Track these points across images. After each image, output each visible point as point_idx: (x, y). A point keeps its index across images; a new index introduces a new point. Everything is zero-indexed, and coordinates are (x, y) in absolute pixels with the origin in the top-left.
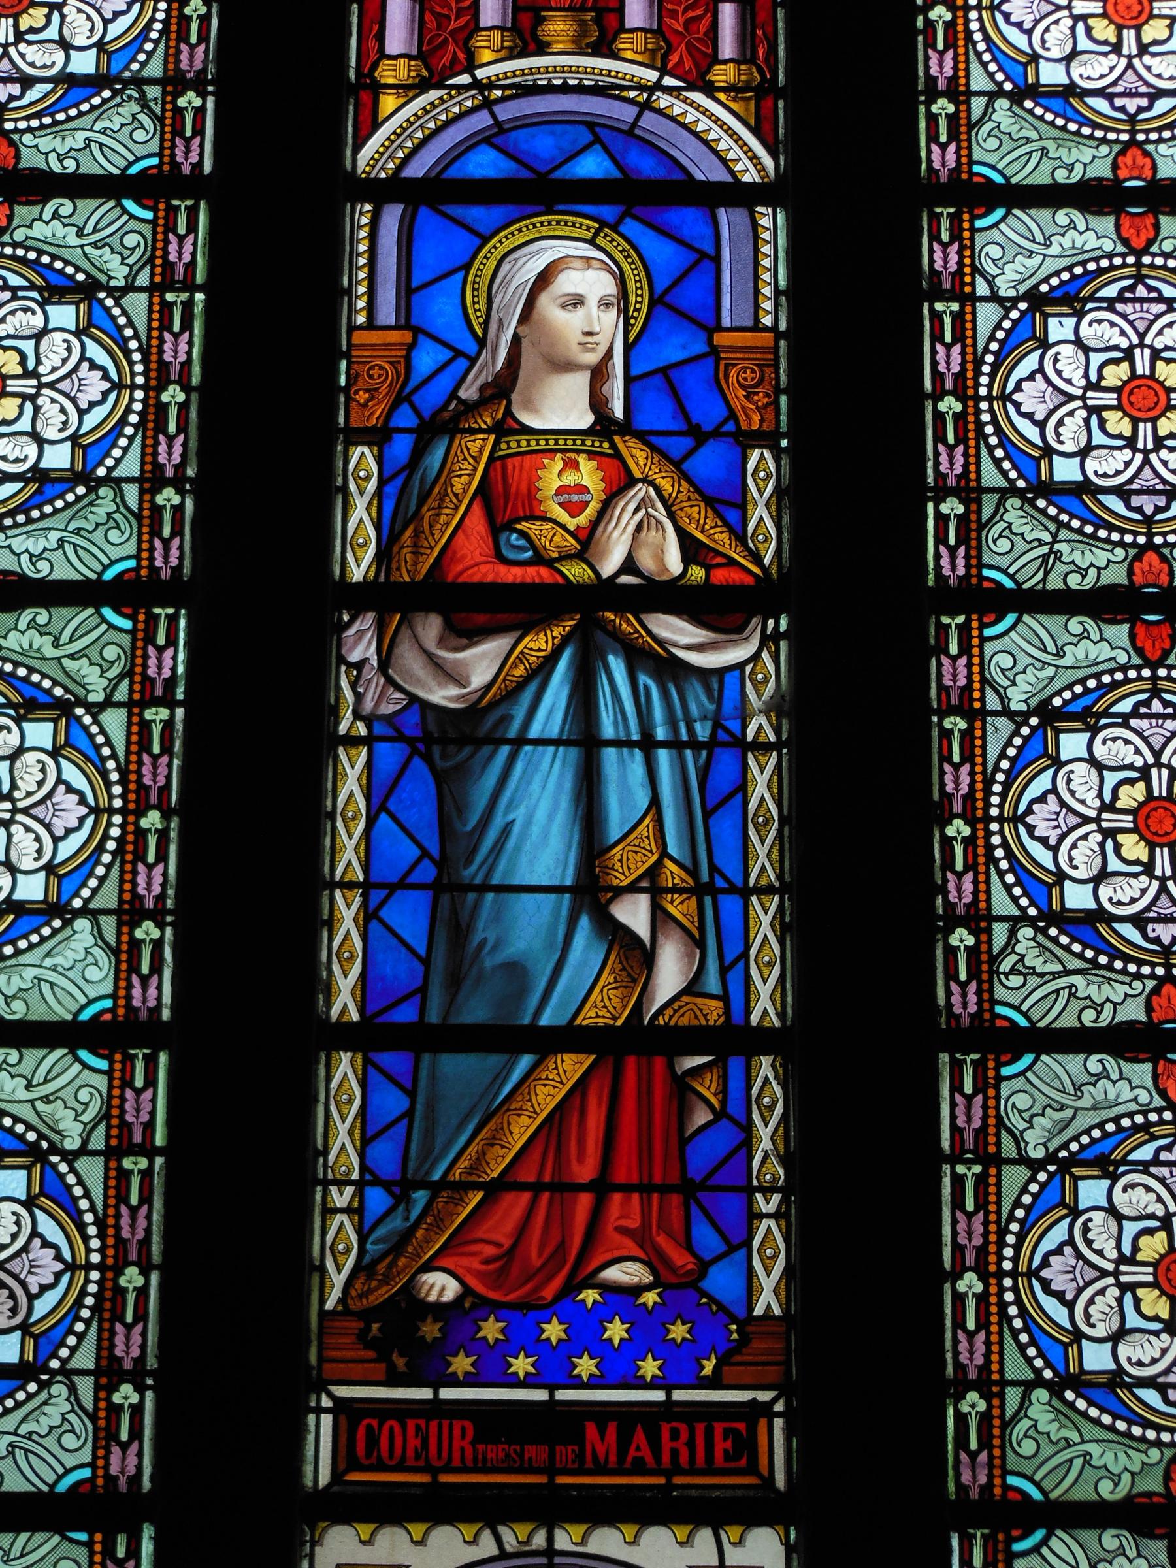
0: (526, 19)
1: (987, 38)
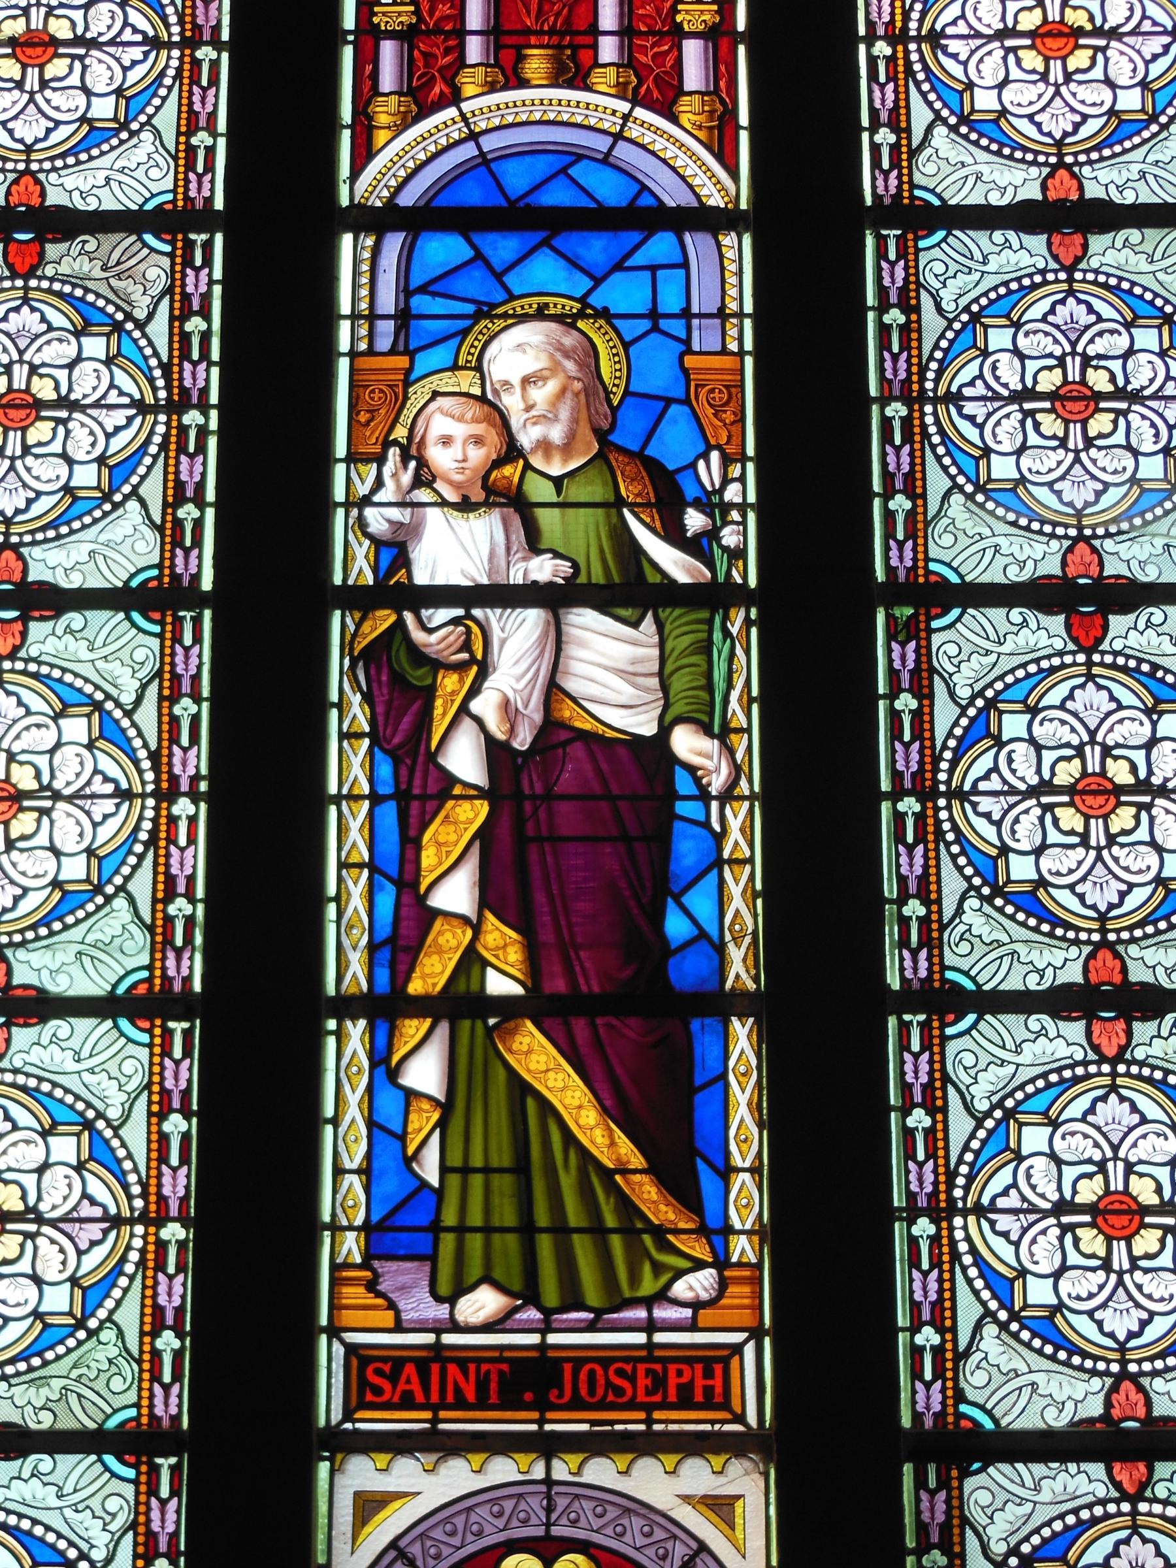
0: (508, 56)
1: (941, 432)
